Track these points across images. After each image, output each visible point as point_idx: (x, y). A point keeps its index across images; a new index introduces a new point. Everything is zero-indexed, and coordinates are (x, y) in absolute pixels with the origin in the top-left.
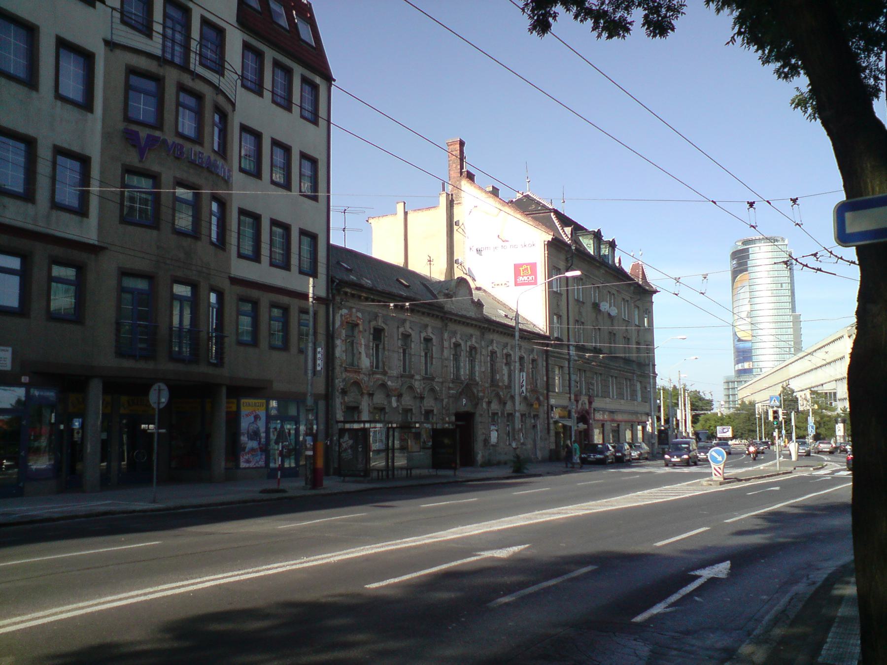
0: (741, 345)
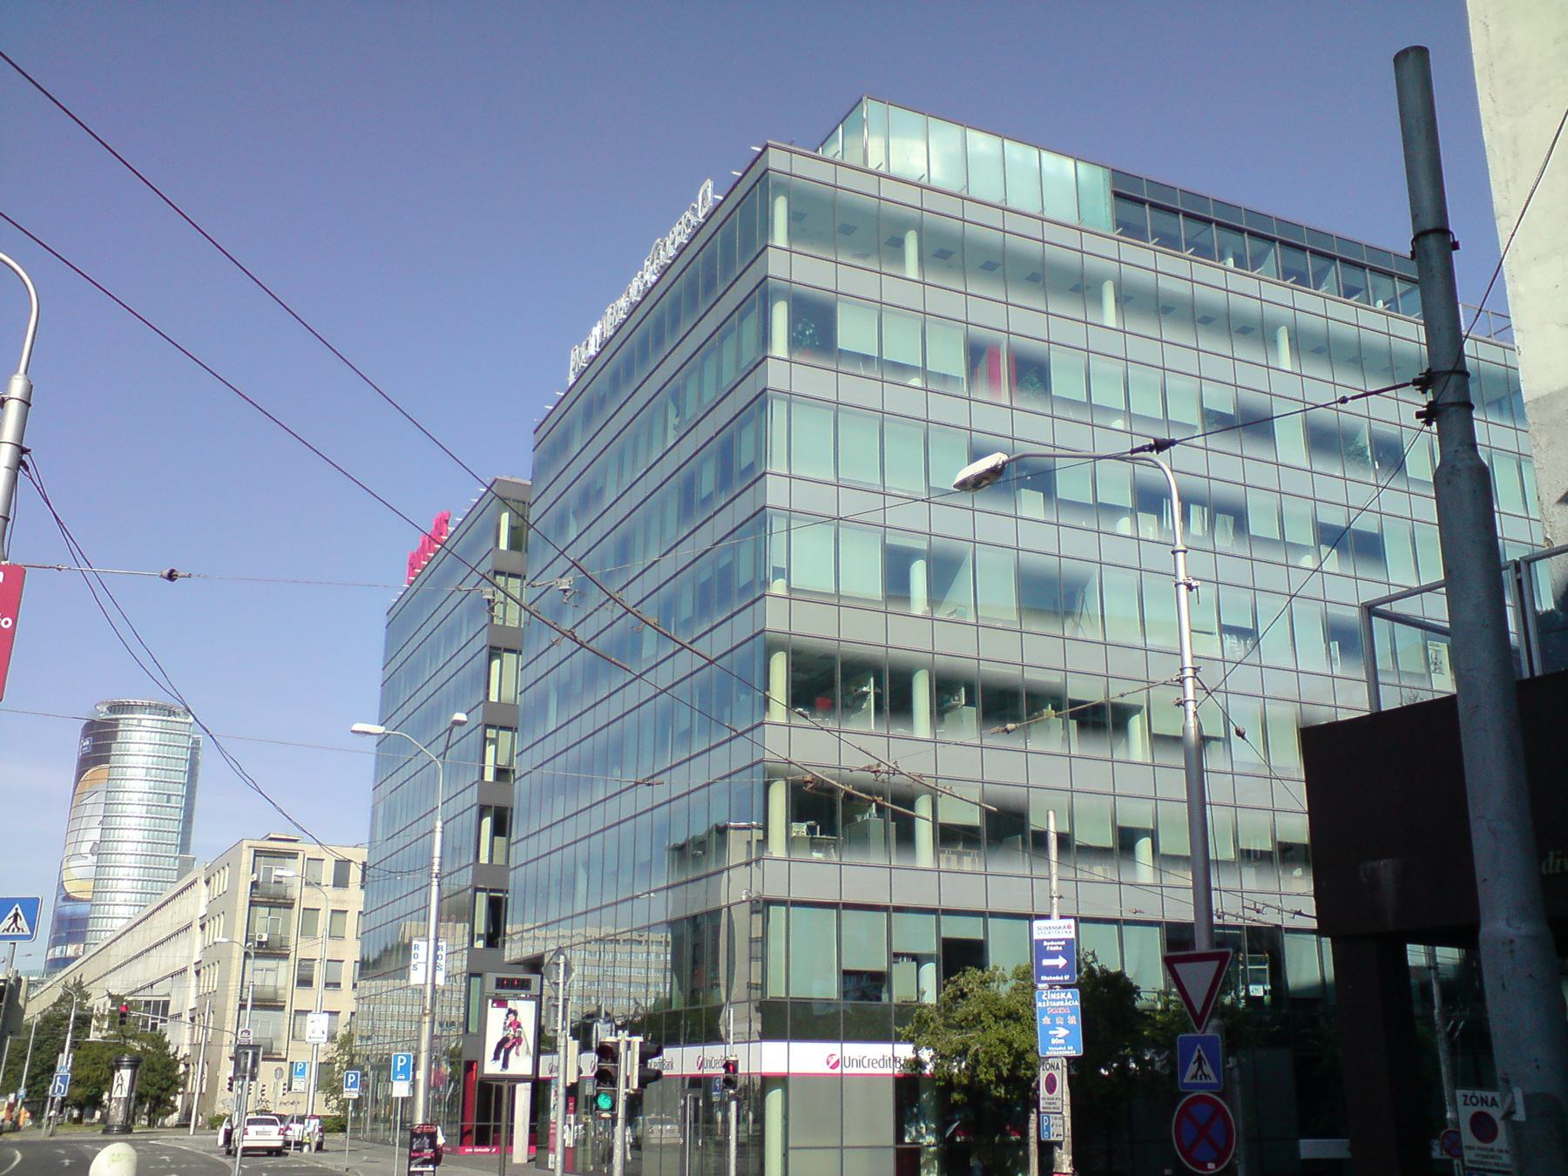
0: (69, 908)
